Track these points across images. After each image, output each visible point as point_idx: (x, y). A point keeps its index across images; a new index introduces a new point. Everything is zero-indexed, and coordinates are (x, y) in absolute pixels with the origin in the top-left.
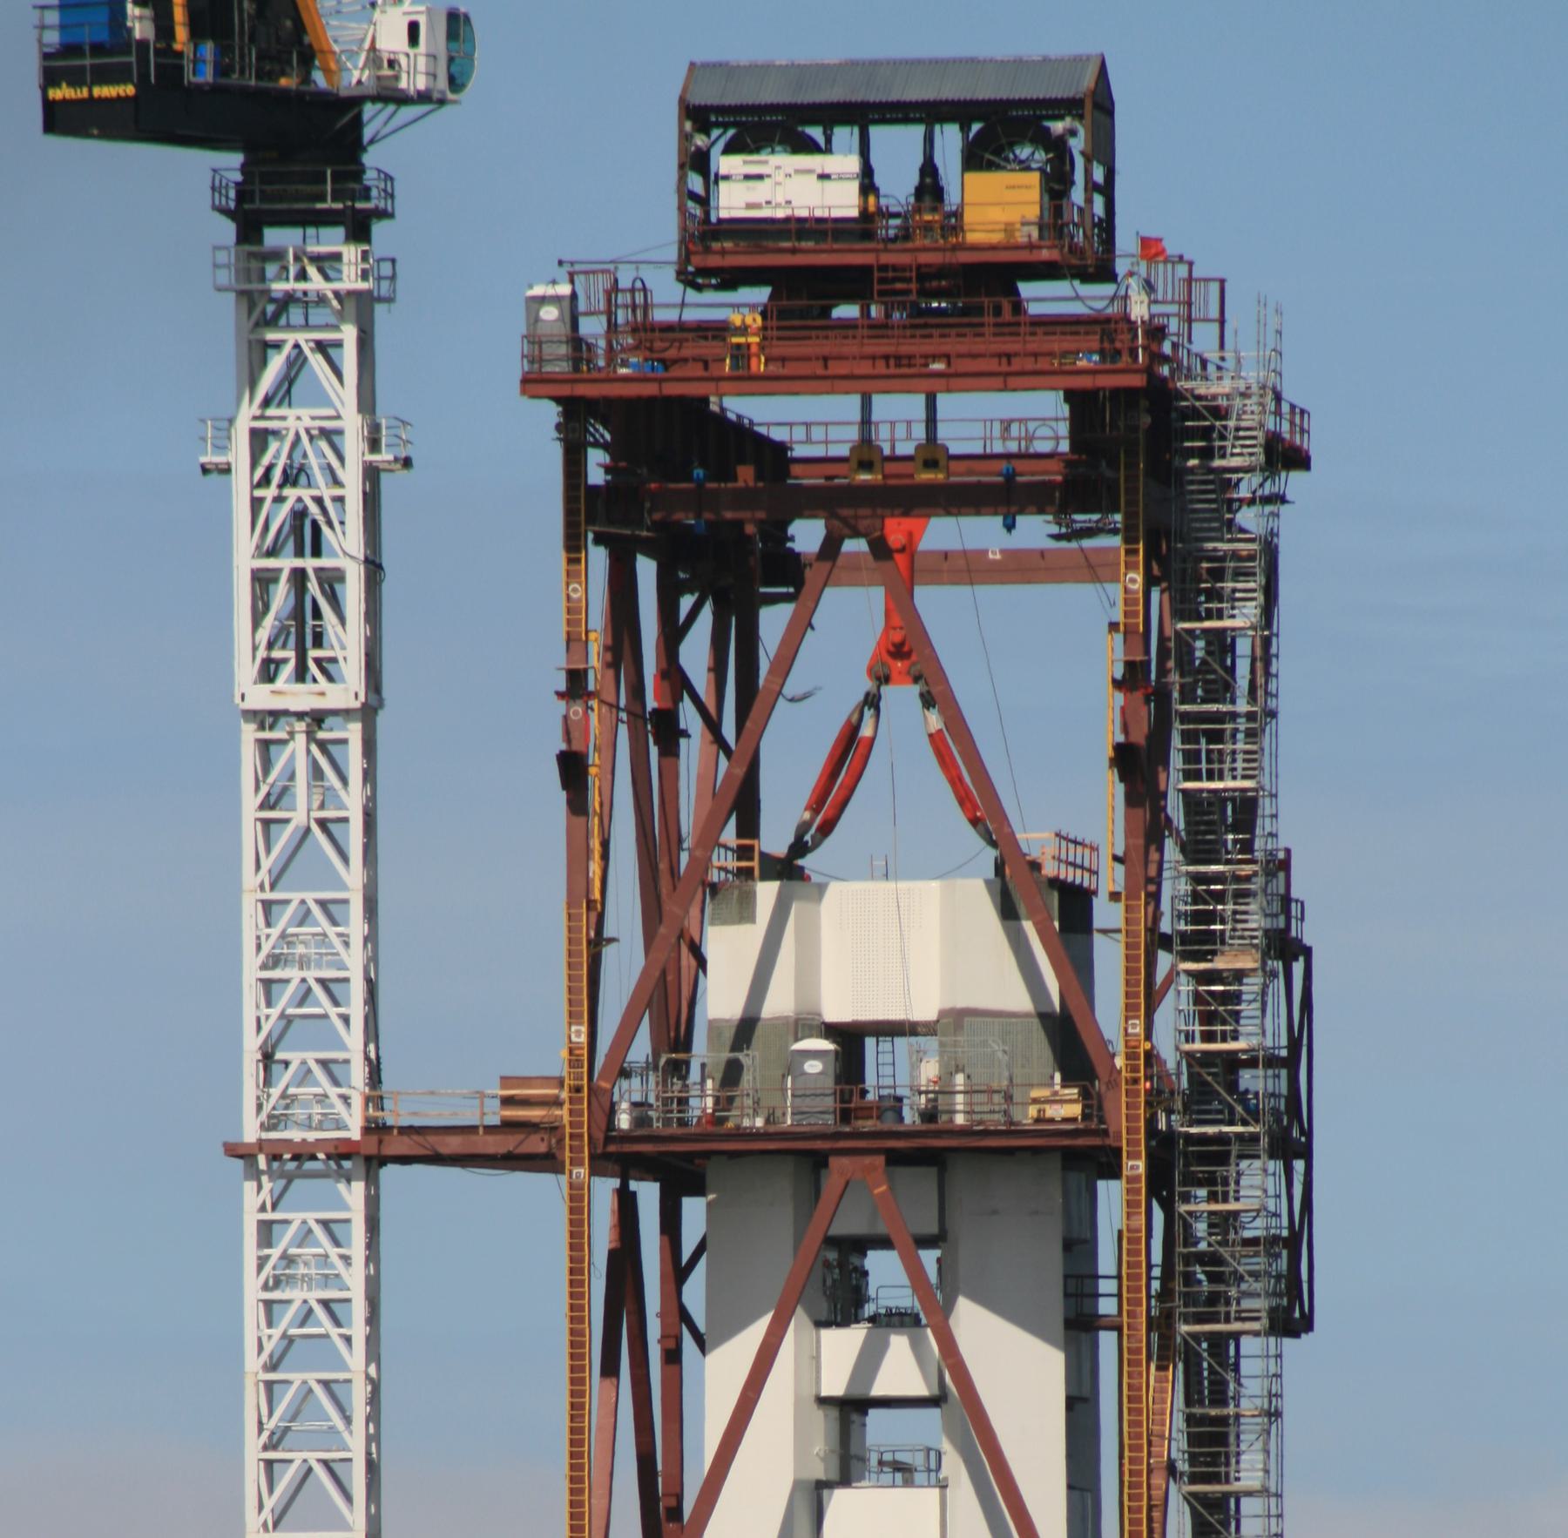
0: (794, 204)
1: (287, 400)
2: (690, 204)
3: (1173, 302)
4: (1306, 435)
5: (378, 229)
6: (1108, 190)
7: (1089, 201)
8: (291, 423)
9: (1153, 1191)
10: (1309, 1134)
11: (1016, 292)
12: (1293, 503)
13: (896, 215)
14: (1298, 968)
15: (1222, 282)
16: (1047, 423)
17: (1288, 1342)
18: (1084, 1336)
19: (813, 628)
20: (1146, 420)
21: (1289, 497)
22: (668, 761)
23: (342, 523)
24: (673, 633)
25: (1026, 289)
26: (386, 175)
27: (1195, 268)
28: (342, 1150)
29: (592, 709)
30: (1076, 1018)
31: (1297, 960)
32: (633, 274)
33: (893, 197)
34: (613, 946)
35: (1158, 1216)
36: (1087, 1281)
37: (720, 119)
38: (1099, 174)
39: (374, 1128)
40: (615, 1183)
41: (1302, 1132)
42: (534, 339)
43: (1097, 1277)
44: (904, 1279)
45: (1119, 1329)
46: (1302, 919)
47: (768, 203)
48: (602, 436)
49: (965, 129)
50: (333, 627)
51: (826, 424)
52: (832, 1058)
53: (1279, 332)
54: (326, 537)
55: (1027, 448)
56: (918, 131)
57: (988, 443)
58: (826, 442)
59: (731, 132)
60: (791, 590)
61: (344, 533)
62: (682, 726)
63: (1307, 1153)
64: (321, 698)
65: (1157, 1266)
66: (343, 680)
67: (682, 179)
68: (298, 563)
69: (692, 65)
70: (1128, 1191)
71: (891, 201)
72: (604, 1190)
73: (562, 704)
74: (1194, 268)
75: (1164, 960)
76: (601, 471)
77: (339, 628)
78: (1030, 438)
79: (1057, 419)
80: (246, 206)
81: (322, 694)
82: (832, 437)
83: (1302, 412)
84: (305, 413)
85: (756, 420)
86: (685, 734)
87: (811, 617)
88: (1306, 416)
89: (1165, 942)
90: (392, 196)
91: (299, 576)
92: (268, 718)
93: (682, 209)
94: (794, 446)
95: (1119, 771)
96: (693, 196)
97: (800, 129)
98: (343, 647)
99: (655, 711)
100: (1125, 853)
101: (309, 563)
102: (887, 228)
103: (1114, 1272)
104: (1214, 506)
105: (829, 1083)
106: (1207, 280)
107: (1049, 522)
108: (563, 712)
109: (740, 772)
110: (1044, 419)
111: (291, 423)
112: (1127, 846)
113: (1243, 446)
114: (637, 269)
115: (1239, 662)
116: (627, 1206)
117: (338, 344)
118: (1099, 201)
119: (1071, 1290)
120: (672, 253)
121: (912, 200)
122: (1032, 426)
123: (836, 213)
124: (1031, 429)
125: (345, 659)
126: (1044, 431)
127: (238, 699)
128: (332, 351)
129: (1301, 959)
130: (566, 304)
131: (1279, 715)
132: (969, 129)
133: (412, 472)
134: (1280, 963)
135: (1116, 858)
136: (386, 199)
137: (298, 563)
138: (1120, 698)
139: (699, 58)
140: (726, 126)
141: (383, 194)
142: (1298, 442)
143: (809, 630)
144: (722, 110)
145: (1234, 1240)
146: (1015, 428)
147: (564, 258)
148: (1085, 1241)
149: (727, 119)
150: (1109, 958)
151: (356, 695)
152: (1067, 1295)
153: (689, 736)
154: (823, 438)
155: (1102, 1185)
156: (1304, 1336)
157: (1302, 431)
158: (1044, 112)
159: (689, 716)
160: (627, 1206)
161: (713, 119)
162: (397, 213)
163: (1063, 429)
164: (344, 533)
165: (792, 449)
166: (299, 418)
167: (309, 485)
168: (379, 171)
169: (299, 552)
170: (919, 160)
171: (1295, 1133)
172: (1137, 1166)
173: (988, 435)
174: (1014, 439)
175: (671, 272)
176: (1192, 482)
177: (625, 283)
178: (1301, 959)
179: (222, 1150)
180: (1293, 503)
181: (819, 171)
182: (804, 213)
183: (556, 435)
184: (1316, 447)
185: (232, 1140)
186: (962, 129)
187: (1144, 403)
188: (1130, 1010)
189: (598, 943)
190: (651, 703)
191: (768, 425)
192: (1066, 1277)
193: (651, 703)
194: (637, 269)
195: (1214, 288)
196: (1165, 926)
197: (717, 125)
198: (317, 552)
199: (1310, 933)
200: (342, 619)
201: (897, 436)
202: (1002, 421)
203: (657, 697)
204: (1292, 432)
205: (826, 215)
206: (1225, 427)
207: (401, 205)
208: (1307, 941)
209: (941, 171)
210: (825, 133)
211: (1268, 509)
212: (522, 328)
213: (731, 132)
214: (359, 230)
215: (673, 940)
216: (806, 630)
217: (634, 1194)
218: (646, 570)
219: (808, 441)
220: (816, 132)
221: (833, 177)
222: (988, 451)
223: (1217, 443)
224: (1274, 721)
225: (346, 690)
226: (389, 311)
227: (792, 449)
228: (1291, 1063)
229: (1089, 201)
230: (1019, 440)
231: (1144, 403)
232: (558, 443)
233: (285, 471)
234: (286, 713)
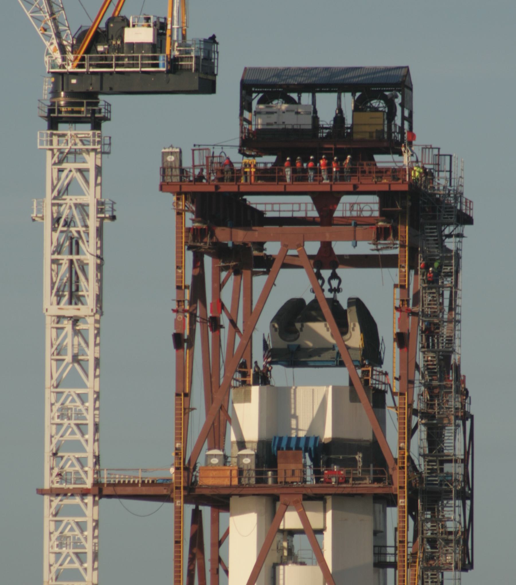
0: (286, 123)
1: (66, 193)
2: (245, 123)
3: (431, 164)
5: (104, 125)
6: (410, 119)
7: (403, 124)
8: (68, 201)
9: (410, 513)
10: (472, 490)
11: (373, 159)
13: (326, 128)
14: (468, 423)
15: (451, 156)
16: (368, 204)
17: (463, 574)
18: (381, 570)
19: (275, 285)
20: (409, 204)
21: (465, 235)
23: (88, 241)
24: (219, 286)
25: (377, 158)
26: (108, 103)
27: (441, 150)
28: (84, 492)
29: (186, 316)
32: (220, 150)
33: (325, 121)
34: (195, 411)
35: (411, 522)
36: (383, 548)
37: (256, 90)
38: (406, 114)
39: (97, 484)
40: (193, 506)
41: (469, 489)
43: (386, 547)
44: (310, 547)
45: (396, 568)
46: (470, 404)
47: (276, 123)
48: (192, 208)
49: (353, 95)
50: (83, 283)
53: (462, 170)
54: (82, 248)
55: (360, 214)
56: (335, 95)
58: (280, 211)
59: (261, 95)
60: (265, 270)
61: (88, 246)
62: (222, 323)
63: (471, 498)
64: (78, 311)
65: (410, 542)
66: (87, 304)
67: (241, 114)
68: (70, 257)
69: (246, 68)
70: (400, 511)
71: (324, 123)
72: (189, 509)
73: (175, 314)
75: (415, 420)
76: (191, 222)
77: (86, 283)
78: (361, 211)
79: (374, 203)
80: (52, 115)
81: (79, 309)
82: (281, 209)
83: (470, 202)
84: (73, 198)
86: (222, 327)
87: (274, 281)
88: (471, 204)
89: (415, 412)
90: (110, 112)
91: (71, 262)
92: (60, 318)
93: (242, 125)
96: (245, 120)
97: (288, 94)
98: (87, 291)
99: (211, 317)
101: (75, 257)
102: (323, 133)
103: (393, 545)
104: (436, 238)
106: (445, 155)
107: (370, 244)
108: (175, 317)
109: (245, 342)
110: (367, 203)
111: (68, 201)
112: (400, 373)
114: (222, 148)
116: (197, 516)
117: (87, 170)
118: (406, 124)
119: (377, 552)
120: (237, 142)
121: (332, 123)
123: (303, 127)
124: (362, 207)
125: (88, 296)
126: (367, 208)
127: (45, 311)
128: (85, 173)
129: (469, 420)
130: (178, 154)
132: (355, 95)
133: (116, 221)
136: (108, 113)
137: (70, 257)
138: (398, 314)
139: (249, 65)
140: (259, 92)
141: (106, 111)
142: (468, 213)
143: (274, 286)
144: (257, 86)
145: (442, 532)
146: (356, 207)
147: (196, 143)
148: (382, 532)
149: (259, 90)
151: (92, 310)
152: (375, 554)
153: (224, 328)
154: (278, 209)
155: (389, 510)
156: (469, 571)
158: (385, 89)
159: (224, 320)
160: (197, 516)
161: (253, 89)
162: (112, 118)
163: (376, 207)
164: (88, 246)
165: (266, 214)
166: (71, 200)
167: (75, 226)
168: (105, 102)
169: (71, 253)
170: (335, 107)
171: (467, 489)
172: (403, 502)
173: (344, 209)
175: (236, 150)
178: (469, 420)
179: (35, 492)
181: (296, 110)
182: (290, 127)
183: (173, 207)
184: (475, 215)
185: (40, 487)
186: (352, 95)
188: (401, 439)
189: (188, 410)
190: (209, 315)
191: (256, 204)
192: (375, 547)
194: (222, 148)
196: (415, 406)
197: (255, 92)
198: (78, 253)
199: (473, 409)
200: (87, 279)
202: (350, 203)
203: (212, 311)
204: (466, 209)
205: (299, 127)
207: (113, 115)
208: (472, 413)
209: (344, 112)
210: (298, 96)
211: (458, 239)
212: (161, 165)
213: (261, 95)
214: (96, 125)
217: (201, 511)
218: (208, 260)
219: (273, 211)
220: (295, 96)
221: (301, 113)
222: (344, 215)
224: (459, 324)
225: (88, 308)
226: (108, 157)
228: (465, 461)
229: (403, 124)
230: (357, 211)
233: (65, 220)
234: (64, 317)
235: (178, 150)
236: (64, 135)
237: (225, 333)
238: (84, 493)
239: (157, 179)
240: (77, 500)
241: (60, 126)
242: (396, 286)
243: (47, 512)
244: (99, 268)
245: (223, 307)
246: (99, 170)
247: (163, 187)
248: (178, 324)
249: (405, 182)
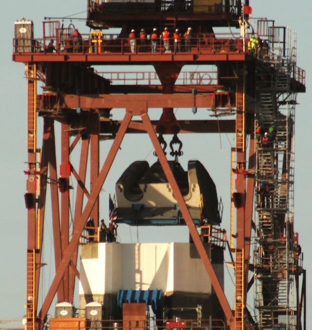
3: (266, 36)
4: (304, 80)
11: (212, 31)
12: (299, 104)
14: (301, 278)
15: (285, 28)
19: (120, 149)
21: (297, 102)
22: (31, 192)
24: (68, 150)
25: (216, 30)
29: (38, 178)
30: (218, 295)
31: (300, 275)
32: (70, 23)
42: (16, 42)
46: (303, 260)
51: (125, 73)
52: (100, 310)
55: (200, 82)
57: (185, 80)
60: (111, 134)
62: (71, 184)
74: (275, 23)
75: (251, 274)
76: (42, 89)
78: (201, 79)
79: (213, 72)
83: (303, 71)
85: (98, 71)
86: (71, 187)
88: (304, 72)
89: (251, 267)
94: (112, 81)
95: (235, 204)
99: (60, 179)
100: (237, 234)
102: (165, 7)
105: (100, 318)
106: (279, 27)
107: (209, 110)
109: (93, 202)
110: (206, 72)
112: (237, 231)
113: (282, 83)
114: (71, 21)
115: (279, 163)
122: (201, 75)
126: (206, 76)
129: (302, 274)
130: (30, 27)
131: (295, 183)
134: (294, 276)
135: (233, 236)
138: (235, 176)
143: (119, 149)
146: (196, 76)
147: (47, 17)
150: (229, 271)
153: (73, 188)
157: (303, 78)
159: (73, 181)
163: (215, 76)
173: (185, 78)
174: (195, 79)
175: (84, 22)
176: (262, 96)
177: (66, 26)
178: (302, 274)
180: (299, 104)
187: (245, 67)
188: (238, 292)
189: (39, 265)
190: (59, 176)
191: (103, 73)
193: (59, 176)
195: (282, 30)
196: (251, 262)
201: (151, 78)
202: (191, 72)
203: (61, 173)
204: (299, 78)
206: (275, 76)
208: (304, 268)
211: (291, 106)
215: (67, 264)
216: (117, 150)
218: (58, 126)
219: (118, 79)
222: (185, 84)
223: (213, 46)
227: (112, 82)
228: (298, 313)
231: (245, 67)
232: (25, 79)
237: (73, 194)
245: (72, 169)
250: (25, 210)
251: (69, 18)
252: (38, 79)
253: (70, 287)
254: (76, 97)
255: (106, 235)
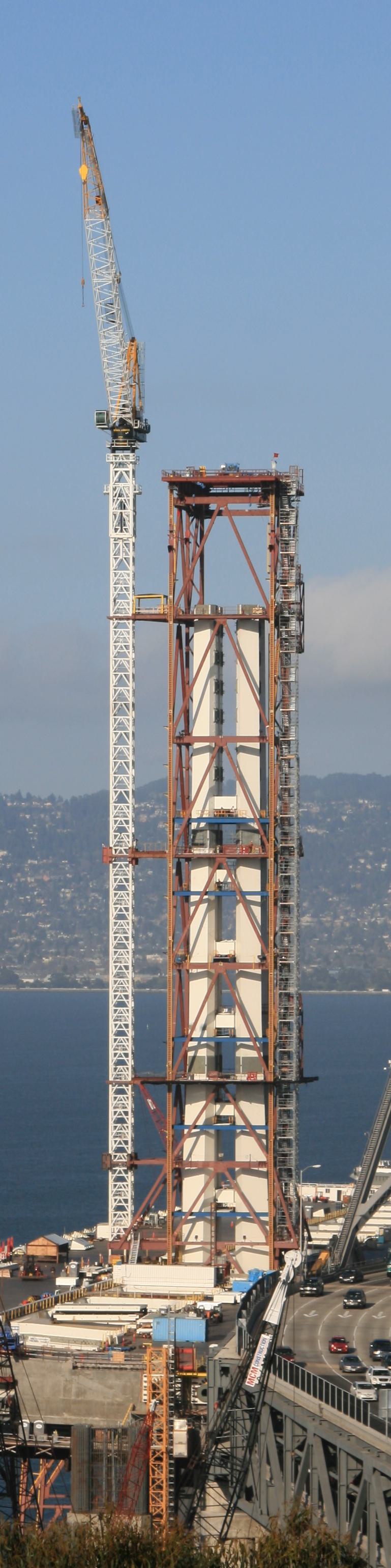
12: (20, 790)
14: (302, 586)
17: (299, 654)
68: (121, 511)
75: (278, 585)
83: (369, 1483)
86: (190, 543)
91: (121, 513)
101: (123, 511)
116: (179, 629)
159: (192, 540)
160: (179, 629)
169: (121, 509)
184: (305, 491)
190: (185, 537)
199: (304, 580)
208: (304, 581)
228: (300, 604)
235: (182, 816)
236: (118, 456)
237: (192, 546)
238: (128, 619)
239: (161, 476)
240: (126, 621)
241: (116, 451)
242: (269, 524)
243: (112, 627)
244: (134, 517)
245: (191, 534)
246: (134, 472)
247: (175, 820)
248: (170, 541)
249: (320, 1291)
250: (168, 554)
251: (267, 1489)
252: (344, 1227)
253: (236, 643)
254: (252, 1161)
255: (133, 1562)
